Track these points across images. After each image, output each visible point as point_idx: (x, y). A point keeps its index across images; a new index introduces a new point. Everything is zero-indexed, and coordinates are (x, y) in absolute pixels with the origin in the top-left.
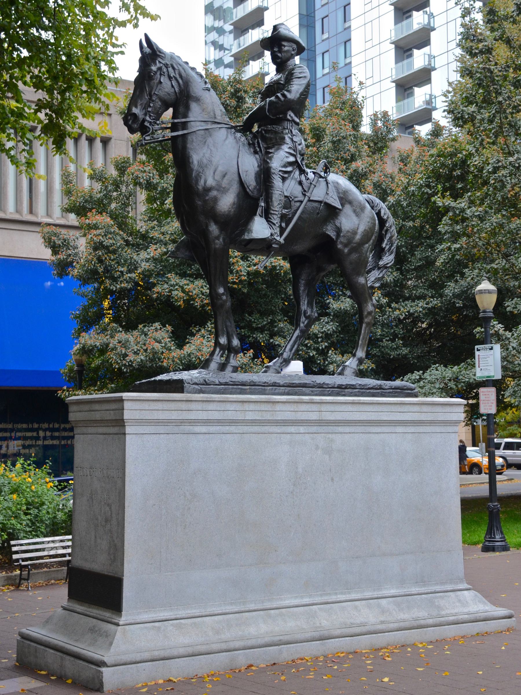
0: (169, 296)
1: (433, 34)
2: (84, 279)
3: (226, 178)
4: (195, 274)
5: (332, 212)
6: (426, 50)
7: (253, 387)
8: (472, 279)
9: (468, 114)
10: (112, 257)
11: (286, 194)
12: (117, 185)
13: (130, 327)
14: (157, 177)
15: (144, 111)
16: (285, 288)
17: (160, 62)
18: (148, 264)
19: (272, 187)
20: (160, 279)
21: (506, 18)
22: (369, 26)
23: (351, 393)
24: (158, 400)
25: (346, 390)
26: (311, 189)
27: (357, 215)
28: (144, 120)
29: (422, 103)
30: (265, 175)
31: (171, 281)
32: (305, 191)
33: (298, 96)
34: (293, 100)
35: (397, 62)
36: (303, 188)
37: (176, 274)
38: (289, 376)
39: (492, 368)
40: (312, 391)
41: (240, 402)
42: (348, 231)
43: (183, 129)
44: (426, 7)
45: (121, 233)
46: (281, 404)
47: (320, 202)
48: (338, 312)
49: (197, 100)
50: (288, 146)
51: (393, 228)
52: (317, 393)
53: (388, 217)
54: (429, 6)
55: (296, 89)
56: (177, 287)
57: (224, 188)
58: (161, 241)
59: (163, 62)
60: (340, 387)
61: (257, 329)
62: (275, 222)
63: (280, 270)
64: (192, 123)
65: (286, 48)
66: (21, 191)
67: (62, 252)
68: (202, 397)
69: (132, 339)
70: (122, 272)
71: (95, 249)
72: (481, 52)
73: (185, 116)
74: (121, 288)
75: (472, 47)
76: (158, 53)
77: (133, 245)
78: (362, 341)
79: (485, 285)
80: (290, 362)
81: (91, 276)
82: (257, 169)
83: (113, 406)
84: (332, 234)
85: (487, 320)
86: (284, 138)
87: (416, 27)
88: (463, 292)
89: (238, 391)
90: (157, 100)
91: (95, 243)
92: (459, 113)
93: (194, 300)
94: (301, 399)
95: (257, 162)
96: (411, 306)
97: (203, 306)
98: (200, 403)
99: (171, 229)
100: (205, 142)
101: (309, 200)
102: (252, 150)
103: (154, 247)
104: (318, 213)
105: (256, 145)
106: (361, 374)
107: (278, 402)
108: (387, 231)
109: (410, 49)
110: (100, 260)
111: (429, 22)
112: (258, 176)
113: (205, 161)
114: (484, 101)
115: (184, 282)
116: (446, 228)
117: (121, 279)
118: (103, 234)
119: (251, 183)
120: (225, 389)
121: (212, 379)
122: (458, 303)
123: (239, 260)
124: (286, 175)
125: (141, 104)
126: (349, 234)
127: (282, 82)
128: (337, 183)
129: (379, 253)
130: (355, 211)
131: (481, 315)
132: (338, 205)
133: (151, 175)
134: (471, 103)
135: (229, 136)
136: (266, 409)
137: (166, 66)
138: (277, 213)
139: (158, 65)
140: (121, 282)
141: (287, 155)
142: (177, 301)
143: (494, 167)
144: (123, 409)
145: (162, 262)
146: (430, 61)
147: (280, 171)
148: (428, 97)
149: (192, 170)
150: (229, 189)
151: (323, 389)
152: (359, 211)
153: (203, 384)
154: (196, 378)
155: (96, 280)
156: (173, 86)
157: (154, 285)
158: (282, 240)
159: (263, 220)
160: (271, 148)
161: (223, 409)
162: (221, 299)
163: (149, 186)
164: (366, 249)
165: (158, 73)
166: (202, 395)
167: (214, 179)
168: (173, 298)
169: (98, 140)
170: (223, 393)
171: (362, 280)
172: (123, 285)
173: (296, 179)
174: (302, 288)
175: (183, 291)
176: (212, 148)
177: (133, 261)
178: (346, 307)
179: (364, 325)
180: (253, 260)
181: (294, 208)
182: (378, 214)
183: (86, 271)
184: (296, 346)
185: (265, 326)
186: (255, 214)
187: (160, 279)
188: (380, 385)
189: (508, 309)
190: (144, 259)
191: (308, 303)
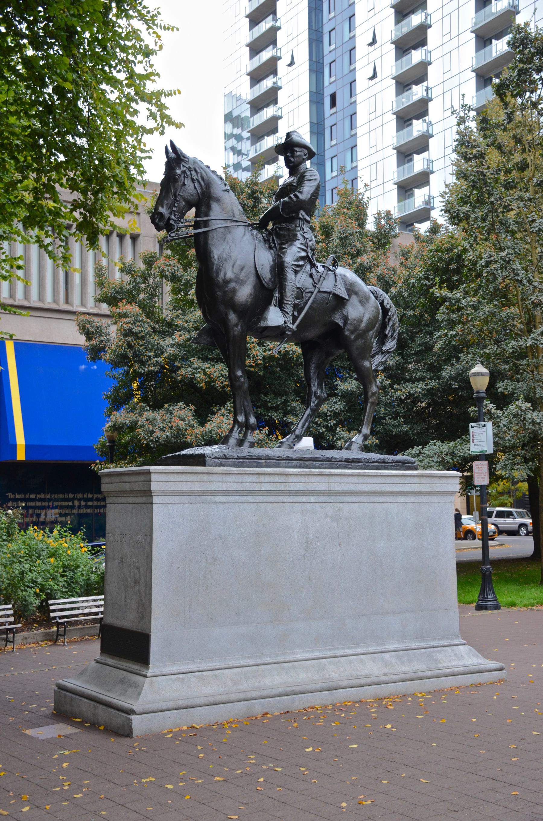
0: (192, 378)
1: (431, 141)
2: (115, 363)
3: (244, 271)
5: (339, 302)
6: (425, 155)
8: (467, 362)
9: (464, 213)
11: (298, 286)
12: (145, 278)
13: (156, 406)
14: (181, 270)
17: (184, 166)
18: (173, 349)
19: (285, 279)
25: (353, 464)
26: (321, 281)
27: (363, 305)
28: (169, 219)
29: (421, 203)
30: (279, 268)
32: (315, 283)
33: (309, 196)
34: (304, 201)
37: (199, 358)
39: (485, 444)
42: (354, 320)
43: (205, 227)
47: (329, 293)
49: (218, 200)
53: (390, 307)
54: (428, 115)
55: (307, 190)
56: (199, 370)
58: (185, 328)
59: (187, 166)
60: (347, 460)
61: (272, 408)
62: (288, 311)
63: (293, 354)
65: (298, 154)
66: (58, 283)
68: (222, 470)
69: (158, 417)
70: (149, 356)
71: (125, 335)
72: (475, 157)
73: (207, 215)
74: (149, 371)
75: (466, 152)
77: (159, 332)
79: (479, 368)
80: (301, 438)
81: (121, 360)
82: (272, 263)
83: (141, 478)
84: (340, 322)
85: (480, 400)
86: (296, 235)
87: (416, 134)
89: (255, 464)
90: (182, 201)
91: (125, 330)
92: (455, 212)
93: (214, 381)
96: (412, 387)
97: (223, 387)
99: (194, 317)
100: (225, 239)
101: (319, 291)
103: (179, 334)
104: (327, 303)
106: (366, 448)
108: (389, 319)
110: (130, 346)
113: (225, 256)
114: (478, 201)
115: (205, 365)
116: (443, 316)
117: (149, 363)
120: (243, 463)
121: (231, 454)
124: (298, 269)
125: (167, 204)
126: (355, 322)
128: (345, 276)
129: (383, 339)
130: (360, 301)
131: (475, 395)
132: (345, 295)
134: (466, 203)
137: (190, 169)
139: (182, 169)
140: (149, 365)
141: (299, 250)
142: (199, 382)
143: (487, 261)
146: (428, 165)
147: (293, 265)
148: (427, 198)
149: (213, 264)
150: (246, 282)
151: (331, 463)
152: (364, 301)
154: (217, 452)
155: (126, 364)
156: (195, 188)
157: (178, 368)
158: (294, 328)
159: (278, 309)
160: (285, 244)
161: (241, 481)
162: (240, 381)
163: (174, 278)
165: (182, 176)
166: (222, 468)
167: (233, 272)
168: (195, 380)
169: (128, 237)
171: (367, 364)
172: (150, 368)
173: (307, 272)
174: (313, 371)
175: (205, 374)
176: (231, 244)
179: (369, 405)
181: (305, 298)
182: (382, 304)
183: (117, 356)
185: (279, 405)
188: (384, 459)
189: (499, 390)
190: (170, 344)
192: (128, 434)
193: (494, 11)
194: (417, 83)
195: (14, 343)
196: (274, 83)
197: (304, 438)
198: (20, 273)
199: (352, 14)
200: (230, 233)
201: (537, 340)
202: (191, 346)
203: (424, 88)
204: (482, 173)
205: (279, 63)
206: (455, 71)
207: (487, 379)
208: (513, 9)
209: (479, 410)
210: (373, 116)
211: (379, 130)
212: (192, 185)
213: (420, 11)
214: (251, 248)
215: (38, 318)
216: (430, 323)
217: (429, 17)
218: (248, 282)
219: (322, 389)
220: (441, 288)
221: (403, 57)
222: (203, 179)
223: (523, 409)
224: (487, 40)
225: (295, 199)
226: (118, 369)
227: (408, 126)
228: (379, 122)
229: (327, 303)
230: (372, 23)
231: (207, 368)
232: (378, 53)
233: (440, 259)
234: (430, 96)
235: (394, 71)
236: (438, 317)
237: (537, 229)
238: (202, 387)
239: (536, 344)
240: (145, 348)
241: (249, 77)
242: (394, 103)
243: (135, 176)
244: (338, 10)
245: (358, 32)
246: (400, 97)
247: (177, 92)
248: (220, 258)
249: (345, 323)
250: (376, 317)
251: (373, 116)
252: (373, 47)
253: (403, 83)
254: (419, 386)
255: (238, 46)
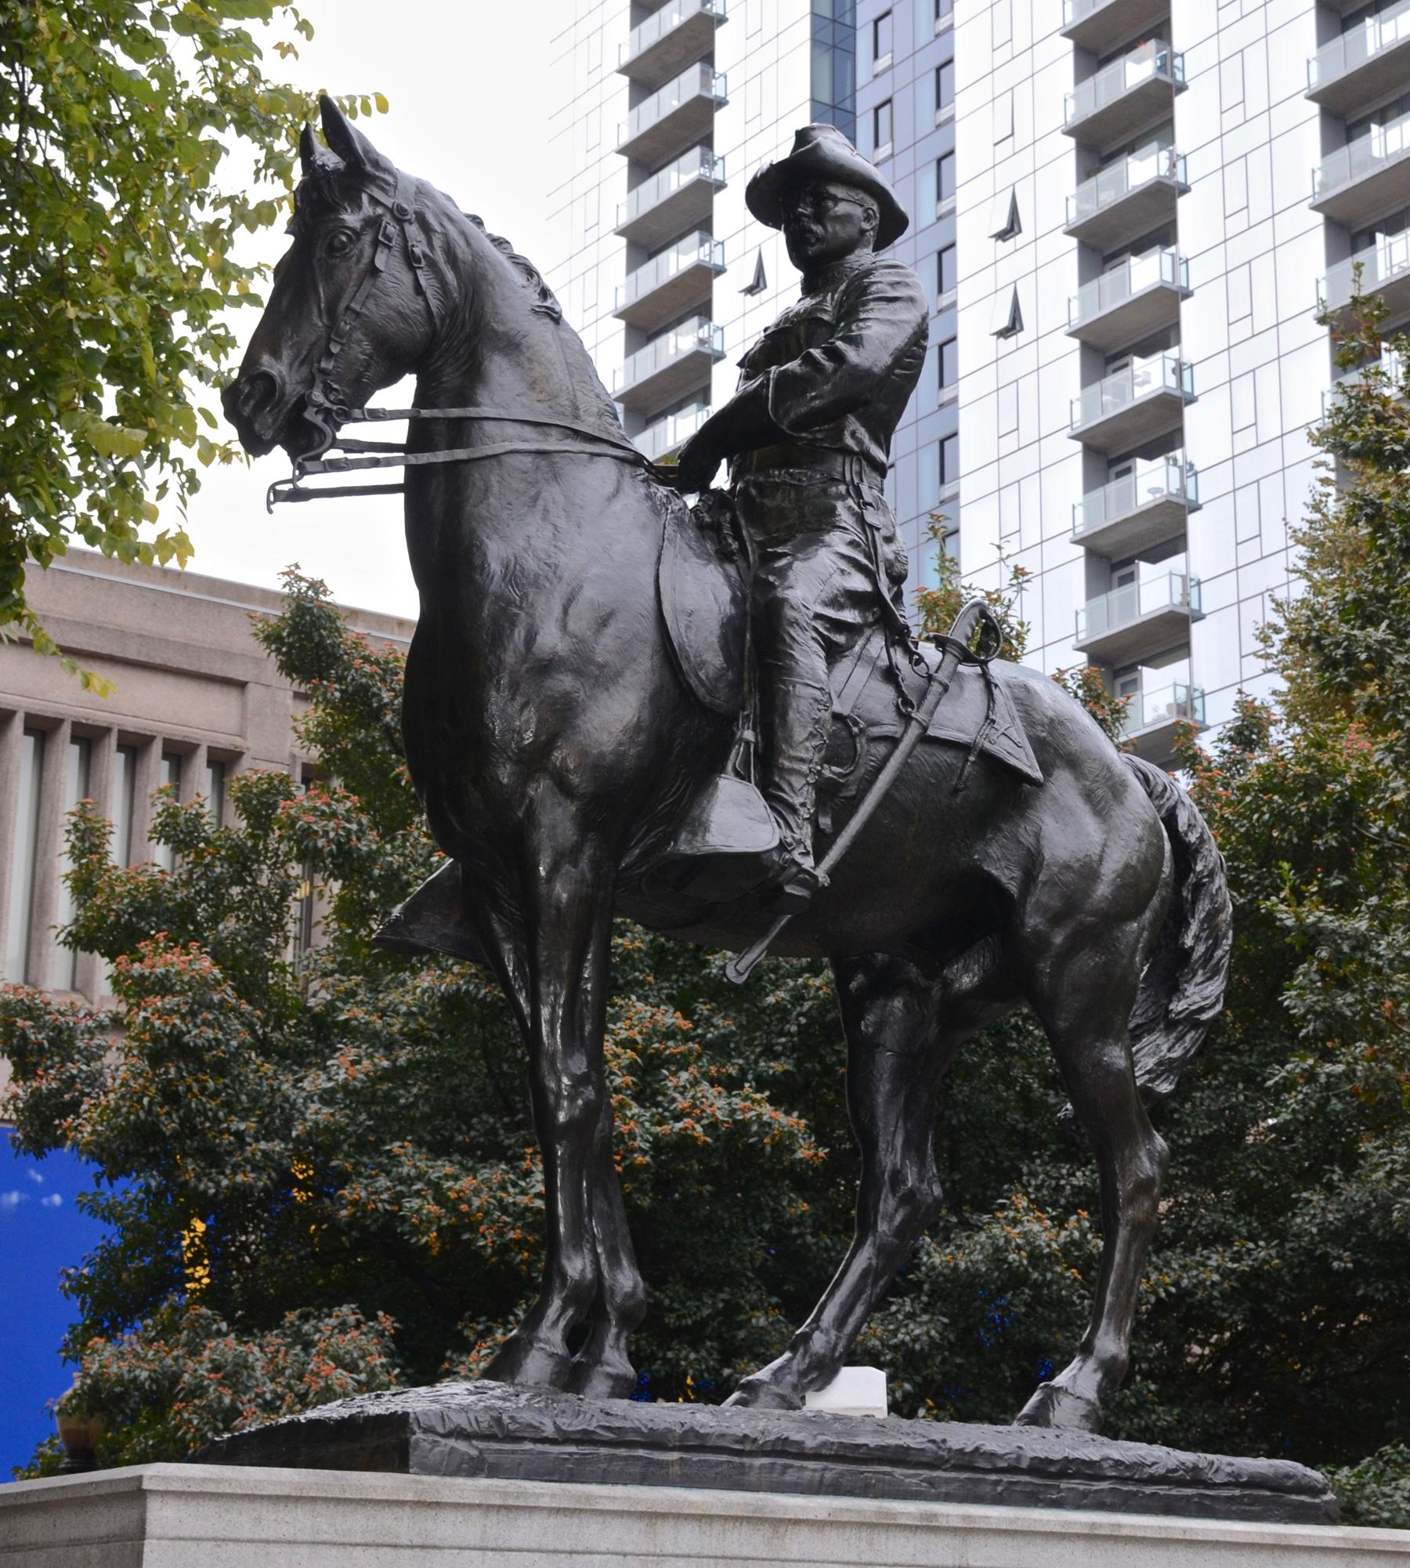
0: (393, 1214)
1: (1193, 520)
3: (611, 630)
4: (479, 1146)
5: (1004, 791)
6: (1176, 562)
7: (696, 1457)
8: (1390, 1175)
9: (1368, 648)
10: (211, 1084)
11: (837, 707)
12: (242, 861)
13: (255, 1316)
14: (373, 835)
15: (305, 370)
17: (374, 201)
18: (326, 1110)
19: (790, 671)
20: (365, 1159)
23: (1085, 1494)
24: (298, 1499)
25: (1064, 1484)
26: (931, 699)
27: (1100, 811)
28: (303, 403)
29: (1163, 711)
30: (758, 629)
31: (401, 1164)
32: (907, 702)
34: (868, 373)
35: (1091, 593)
37: (419, 1144)
38: (836, 1418)
40: (931, 1482)
41: (642, 1515)
42: (1067, 867)
43: (452, 446)
44: (1173, 449)
45: (246, 1007)
46: (804, 1531)
48: (947, 1279)
49: (511, 346)
50: (848, 537)
51: (1220, 880)
52: (951, 1488)
53: (1202, 840)
54: (1182, 445)
55: (877, 338)
56: (418, 1186)
57: (602, 667)
58: (376, 1034)
59: (389, 202)
60: (1040, 1467)
61: (678, 1332)
62: (797, 801)
64: (488, 426)
65: (842, 208)
67: (46, 1070)
68: (486, 1491)
70: (239, 1135)
73: (465, 398)
74: (234, 1187)
75: (1381, 434)
76: (369, 168)
77: (283, 1055)
78: (1116, 1295)
81: (132, 1146)
82: (729, 610)
84: (1007, 875)
86: (834, 508)
87: (1144, 499)
89: (636, 1469)
90: (358, 335)
91: (156, 1039)
92: (1338, 645)
93: (473, 1227)
95: (731, 586)
97: (503, 1249)
98: (475, 1514)
99: (408, 998)
100: (535, 499)
101: (925, 739)
102: (710, 547)
103: (352, 1053)
104: (956, 791)
105: (727, 530)
106: (1107, 1421)
107: (797, 1522)
108: (1198, 887)
109: (1130, 561)
110: (170, 1096)
111: (1183, 489)
112: (731, 632)
113: (531, 565)
116: (1311, 998)
118: (184, 1009)
120: (583, 1459)
121: (526, 1417)
122: (1339, 1258)
123: (628, 1100)
124: (840, 639)
125: (297, 347)
126: (1069, 877)
127: (826, 317)
128: (1026, 688)
130: (1088, 796)
132: (1026, 762)
133: (354, 827)
134: (1372, 620)
135: (627, 482)
136: (747, 1551)
137: (399, 215)
138: (805, 768)
139: (367, 209)
140: (236, 1169)
141: (844, 565)
142: (416, 1230)
144: (141, 1534)
145: (373, 1102)
146: (1185, 594)
147: (818, 616)
148: (1182, 694)
149: (481, 593)
150: (619, 674)
152: (1103, 795)
153: (491, 1437)
154: (464, 1409)
155: (153, 1161)
156: (419, 290)
157: (344, 1178)
158: (821, 874)
159: (751, 792)
160: (784, 542)
161: (568, 1545)
163: (346, 862)
164: (1131, 939)
165: (367, 239)
166: (483, 1482)
167: (564, 627)
168: (404, 1219)
169: (202, 757)
171: (1115, 1055)
172: (240, 1178)
173: (873, 662)
174: (884, 1088)
175: (441, 1199)
176: (561, 523)
177: (278, 1100)
178: (974, 1263)
180: (674, 1100)
181: (865, 764)
183: (122, 1131)
185: (704, 1322)
186: (723, 770)
187: (365, 1159)
188: (1195, 1468)
190: (313, 1093)
192: (146, 1428)
193: (1377, 152)
194: (1146, 348)
196: (702, 342)
197: (847, 1373)
199: (946, 149)
200: (556, 477)
202: (395, 1100)
203: (1171, 364)
205: (718, 283)
211: (1030, 487)
212: (406, 278)
213: (1154, 146)
214: (642, 546)
216: (1241, 1041)
217: (1180, 164)
218: (629, 678)
219: (922, 1165)
221: (1102, 272)
224: (1361, 233)
225: (829, 365)
226: (122, 1182)
227: (1119, 475)
228: (1028, 460)
230: (1006, 175)
231: (447, 1177)
234: (1187, 388)
235: (1075, 313)
236: (1289, 998)
238: (427, 1247)
240: (226, 1104)
242: (1077, 407)
243: (188, 348)
245: (963, 199)
246: (1095, 388)
247: (373, 103)
248: (513, 574)
249: (1029, 878)
252: (1010, 244)
253: (1105, 349)
254: (1212, 1263)
255: (592, 235)
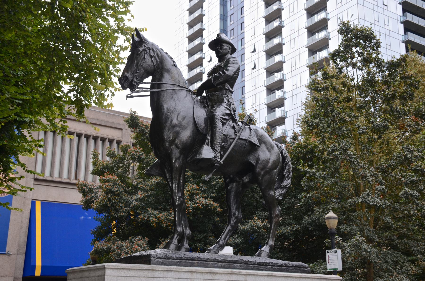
1: (285, 101)
2: (100, 210)
3: (185, 120)
4: (163, 208)
5: (253, 148)
6: (282, 108)
7: (200, 262)
8: (319, 213)
9: (316, 123)
11: (224, 133)
12: (122, 160)
13: (124, 238)
15: (133, 75)
16: (214, 217)
17: (145, 46)
19: (216, 127)
21: (333, 77)
22: (254, 97)
23: (267, 268)
25: (263, 267)
26: (240, 132)
27: (269, 151)
29: (280, 134)
30: (211, 120)
32: (236, 132)
33: (233, 73)
34: (230, 76)
36: (235, 131)
37: (152, 208)
38: (224, 255)
39: (336, 264)
40: (240, 266)
41: (191, 272)
42: (264, 161)
45: (123, 185)
46: (219, 274)
47: (246, 140)
49: (168, 71)
52: (244, 267)
53: (287, 156)
55: (231, 70)
57: (184, 126)
58: (145, 189)
59: (147, 46)
60: (259, 264)
62: (217, 149)
63: (211, 207)
64: (164, 85)
65: (225, 47)
66: (71, 167)
68: (164, 268)
69: (124, 244)
70: (121, 207)
71: (107, 193)
72: (323, 89)
73: (160, 80)
74: (120, 216)
78: (272, 234)
79: (331, 214)
80: (224, 247)
81: (103, 208)
82: (206, 116)
83: (98, 273)
84: (253, 162)
85: (332, 235)
88: (312, 221)
90: (142, 69)
91: (107, 190)
93: (162, 222)
94: (233, 272)
96: (284, 229)
97: (167, 226)
100: (172, 97)
101: (239, 139)
103: (141, 193)
104: (245, 148)
106: (271, 256)
107: (217, 273)
108: (286, 164)
109: (274, 108)
110: (110, 200)
111: (284, 96)
112: (206, 120)
113: (172, 109)
114: (325, 115)
115: (156, 212)
116: (306, 183)
117: (121, 211)
119: (202, 124)
120: (180, 262)
121: (171, 255)
124: (225, 121)
126: (264, 162)
129: (282, 178)
130: (267, 148)
131: (329, 232)
132: (257, 142)
134: (316, 118)
137: (149, 49)
138: (219, 144)
139: (143, 48)
140: (121, 212)
141: (225, 109)
142: (152, 223)
143: (332, 149)
144: (104, 275)
146: (284, 114)
147: (221, 118)
148: (283, 131)
149: (163, 114)
150: (187, 127)
151: (248, 266)
152: (270, 148)
153: (165, 259)
154: (160, 254)
157: (139, 214)
158: (221, 162)
159: (209, 148)
160: (215, 105)
163: (140, 160)
165: (143, 53)
166: (163, 266)
168: (150, 221)
169: (115, 142)
170: (179, 265)
171: (272, 193)
172: (121, 214)
173: (230, 125)
174: (232, 198)
176: (177, 101)
183: (101, 206)
184: (228, 237)
188: (286, 264)
189: (342, 230)
190: (134, 199)
191: (236, 208)
193: (317, 38)
194: (277, 71)
195: (41, 202)
196: (201, 70)
197: (226, 247)
198: (41, 149)
200: (176, 94)
201: (366, 199)
204: (328, 98)
205: (204, 60)
206: (298, 66)
207: (336, 221)
208: (327, 37)
209: (332, 242)
210: (254, 88)
212: (150, 59)
213: (279, 37)
214: (191, 106)
215: (57, 188)
218: (188, 128)
219: (239, 212)
220: (304, 166)
222: (157, 55)
223: (360, 241)
226: (101, 215)
227: (273, 93)
229: (245, 148)
230: (253, 42)
231: (157, 214)
232: (256, 56)
233: (300, 152)
235: (265, 65)
237: (361, 132)
239: (365, 201)
241: (187, 67)
243: (112, 71)
244: (235, 36)
245: (246, 46)
246: (269, 78)
247: (144, 29)
248: (168, 110)
249: (257, 162)
250: (278, 160)
251: (254, 88)
